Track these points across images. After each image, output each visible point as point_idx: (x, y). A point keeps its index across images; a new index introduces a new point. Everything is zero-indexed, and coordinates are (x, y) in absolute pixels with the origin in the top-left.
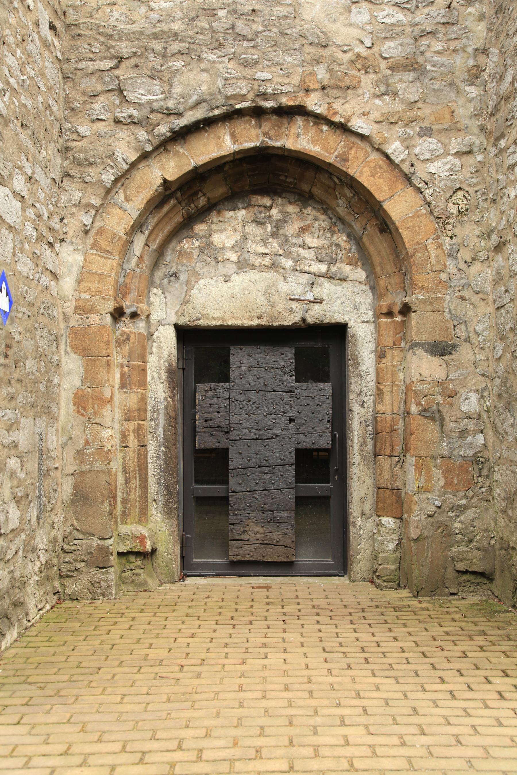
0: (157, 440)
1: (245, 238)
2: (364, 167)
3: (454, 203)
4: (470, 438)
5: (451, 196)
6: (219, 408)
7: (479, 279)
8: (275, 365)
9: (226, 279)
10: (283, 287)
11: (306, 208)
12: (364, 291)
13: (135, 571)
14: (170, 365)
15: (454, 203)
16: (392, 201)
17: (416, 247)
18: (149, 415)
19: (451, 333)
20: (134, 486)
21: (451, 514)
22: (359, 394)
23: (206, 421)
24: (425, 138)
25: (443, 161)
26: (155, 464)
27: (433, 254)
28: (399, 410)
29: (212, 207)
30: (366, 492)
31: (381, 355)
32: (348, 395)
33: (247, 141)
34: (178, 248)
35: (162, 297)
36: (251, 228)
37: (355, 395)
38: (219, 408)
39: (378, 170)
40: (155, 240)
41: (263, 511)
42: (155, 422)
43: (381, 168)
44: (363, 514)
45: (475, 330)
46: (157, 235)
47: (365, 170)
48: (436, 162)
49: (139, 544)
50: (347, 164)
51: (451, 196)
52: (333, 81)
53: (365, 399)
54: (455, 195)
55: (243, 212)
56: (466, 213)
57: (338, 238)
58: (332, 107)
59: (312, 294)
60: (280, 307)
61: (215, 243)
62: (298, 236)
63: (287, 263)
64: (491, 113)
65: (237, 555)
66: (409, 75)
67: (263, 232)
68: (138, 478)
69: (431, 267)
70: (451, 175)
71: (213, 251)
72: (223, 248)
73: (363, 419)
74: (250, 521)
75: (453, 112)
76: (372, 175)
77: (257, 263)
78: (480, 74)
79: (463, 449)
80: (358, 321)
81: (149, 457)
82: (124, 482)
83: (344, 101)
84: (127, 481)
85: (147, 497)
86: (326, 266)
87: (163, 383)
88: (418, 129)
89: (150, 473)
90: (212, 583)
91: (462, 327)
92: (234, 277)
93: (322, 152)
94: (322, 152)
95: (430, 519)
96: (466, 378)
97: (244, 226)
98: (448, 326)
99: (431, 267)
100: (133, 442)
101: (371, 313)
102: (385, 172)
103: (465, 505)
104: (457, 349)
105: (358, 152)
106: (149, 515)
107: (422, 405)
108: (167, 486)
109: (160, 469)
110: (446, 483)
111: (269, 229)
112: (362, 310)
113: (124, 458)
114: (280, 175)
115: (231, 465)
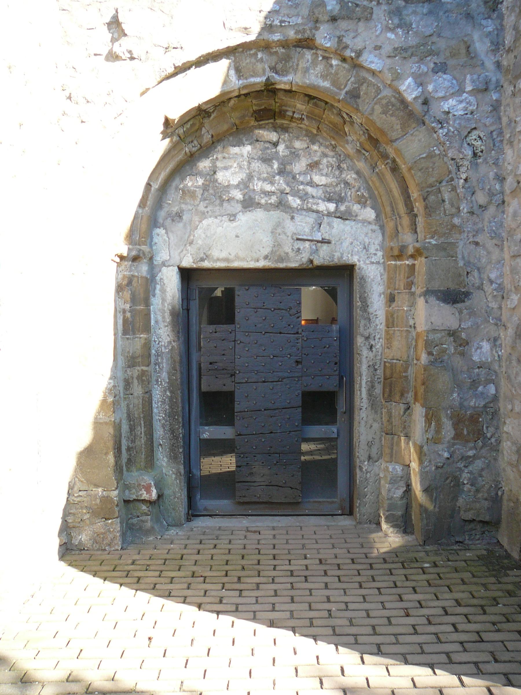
0: (161, 384)
1: (250, 177)
2: (376, 104)
3: (468, 144)
4: (480, 388)
5: (466, 137)
6: (224, 350)
7: (494, 224)
8: (282, 306)
9: (232, 219)
10: (290, 227)
11: (314, 144)
12: (373, 231)
13: (141, 518)
14: (173, 308)
15: (468, 144)
16: (405, 141)
17: (429, 190)
18: (153, 359)
19: (464, 280)
20: (139, 433)
21: (461, 465)
22: (367, 338)
23: (211, 363)
24: (440, 74)
25: (458, 99)
26: (160, 409)
27: (446, 197)
28: (408, 357)
29: (217, 141)
30: (374, 436)
31: (391, 299)
32: (356, 337)
33: (252, 76)
34: (181, 186)
35: (165, 237)
36: (256, 165)
37: (363, 339)
38: (224, 350)
39: (390, 107)
40: (157, 178)
41: (269, 454)
42: (159, 366)
43: (393, 106)
44: (370, 458)
45: (488, 277)
46: (160, 174)
47: (377, 107)
48: (451, 100)
49: (145, 492)
50: (357, 100)
51: (466, 137)
52: (343, 13)
53: (373, 342)
54: (470, 135)
55: (248, 148)
56: (481, 154)
57: (347, 175)
58: (341, 40)
59: (320, 234)
60: (287, 249)
61: (219, 181)
62: (305, 173)
63: (295, 202)
64: (509, 48)
65: (244, 497)
66: (423, 7)
67: (269, 169)
68: (143, 425)
69: (445, 211)
70: (467, 114)
71: (218, 189)
72: (228, 186)
73: (371, 363)
74: (256, 463)
75: (469, 47)
76: (385, 112)
77: (263, 201)
78: (497, 7)
79: (474, 400)
80: (367, 262)
81: (153, 402)
82: (129, 430)
83: (355, 34)
84: (132, 429)
85: (152, 442)
86: (335, 205)
87: (167, 326)
88: (432, 65)
89: (156, 418)
90: (218, 525)
91: (476, 273)
92: (240, 216)
93: (332, 88)
94: (332, 88)
95: (440, 470)
96: (478, 327)
97: (249, 163)
98: (461, 272)
99: (445, 211)
100: (138, 390)
101: (380, 254)
102: (397, 110)
103: (475, 455)
104: (470, 297)
105: (369, 88)
106: (155, 460)
107: (433, 355)
108: (172, 431)
109: (165, 414)
110: (456, 434)
111: (276, 166)
112: (372, 250)
113: (128, 406)
114: (287, 111)
115: (237, 408)
